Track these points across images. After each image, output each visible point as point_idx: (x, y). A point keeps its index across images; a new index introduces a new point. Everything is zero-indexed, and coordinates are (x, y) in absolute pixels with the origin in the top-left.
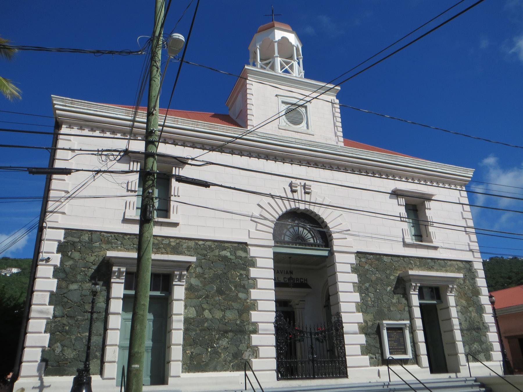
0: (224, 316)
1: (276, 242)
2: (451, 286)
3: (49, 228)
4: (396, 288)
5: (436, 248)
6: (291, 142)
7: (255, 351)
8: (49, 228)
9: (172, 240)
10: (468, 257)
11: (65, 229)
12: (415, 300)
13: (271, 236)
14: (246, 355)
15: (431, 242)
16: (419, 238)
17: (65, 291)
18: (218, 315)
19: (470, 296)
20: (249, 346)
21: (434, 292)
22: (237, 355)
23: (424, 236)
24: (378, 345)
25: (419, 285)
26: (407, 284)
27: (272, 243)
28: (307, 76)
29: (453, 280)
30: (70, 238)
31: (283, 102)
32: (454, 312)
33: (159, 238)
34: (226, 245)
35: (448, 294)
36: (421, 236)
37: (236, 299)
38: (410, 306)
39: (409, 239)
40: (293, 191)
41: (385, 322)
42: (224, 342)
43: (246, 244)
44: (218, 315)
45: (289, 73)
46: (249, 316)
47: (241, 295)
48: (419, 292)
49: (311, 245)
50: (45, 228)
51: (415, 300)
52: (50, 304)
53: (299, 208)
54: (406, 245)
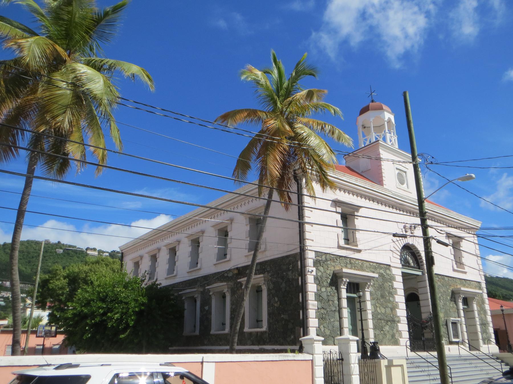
0: (385, 312)
1: (403, 265)
2: (369, 284)
3: (309, 250)
4: (451, 298)
5: (359, 251)
6: (406, 199)
7: (400, 333)
8: (309, 250)
9: (360, 261)
10: (479, 280)
11: (315, 251)
12: (344, 294)
13: (399, 261)
14: (397, 336)
15: (357, 246)
16: (347, 241)
17: (320, 292)
18: (383, 311)
19: (384, 293)
20: (398, 331)
21: (354, 287)
22: (393, 336)
23: (351, 240)
24: (447, 333)
25: (348, 280)
26: (339, 280)
27: (400, 266)
28: (400, 148)
29: (370, 278)
30: (318, 258)
31: (397, 169)
32: (369, 305)
33: (446, 279)
34: (382, 266)
35: (342, 287)
36: (348, 240)
37: (389, 301)
38: (458, 309)
39: (342, 243)
40: (406, 232)
41: (452, 319)
42: (387, 328)
43: (389, 265)
44: (383, 311)
45: (378, 136)
46: (396, 312)
47: (391, 299)
48: (347, 287)
49: (412, 267)
50: (307, 250)
51: (344, 294)
52: (315, 300)
53: (409, 243)
54: (340, 247)
